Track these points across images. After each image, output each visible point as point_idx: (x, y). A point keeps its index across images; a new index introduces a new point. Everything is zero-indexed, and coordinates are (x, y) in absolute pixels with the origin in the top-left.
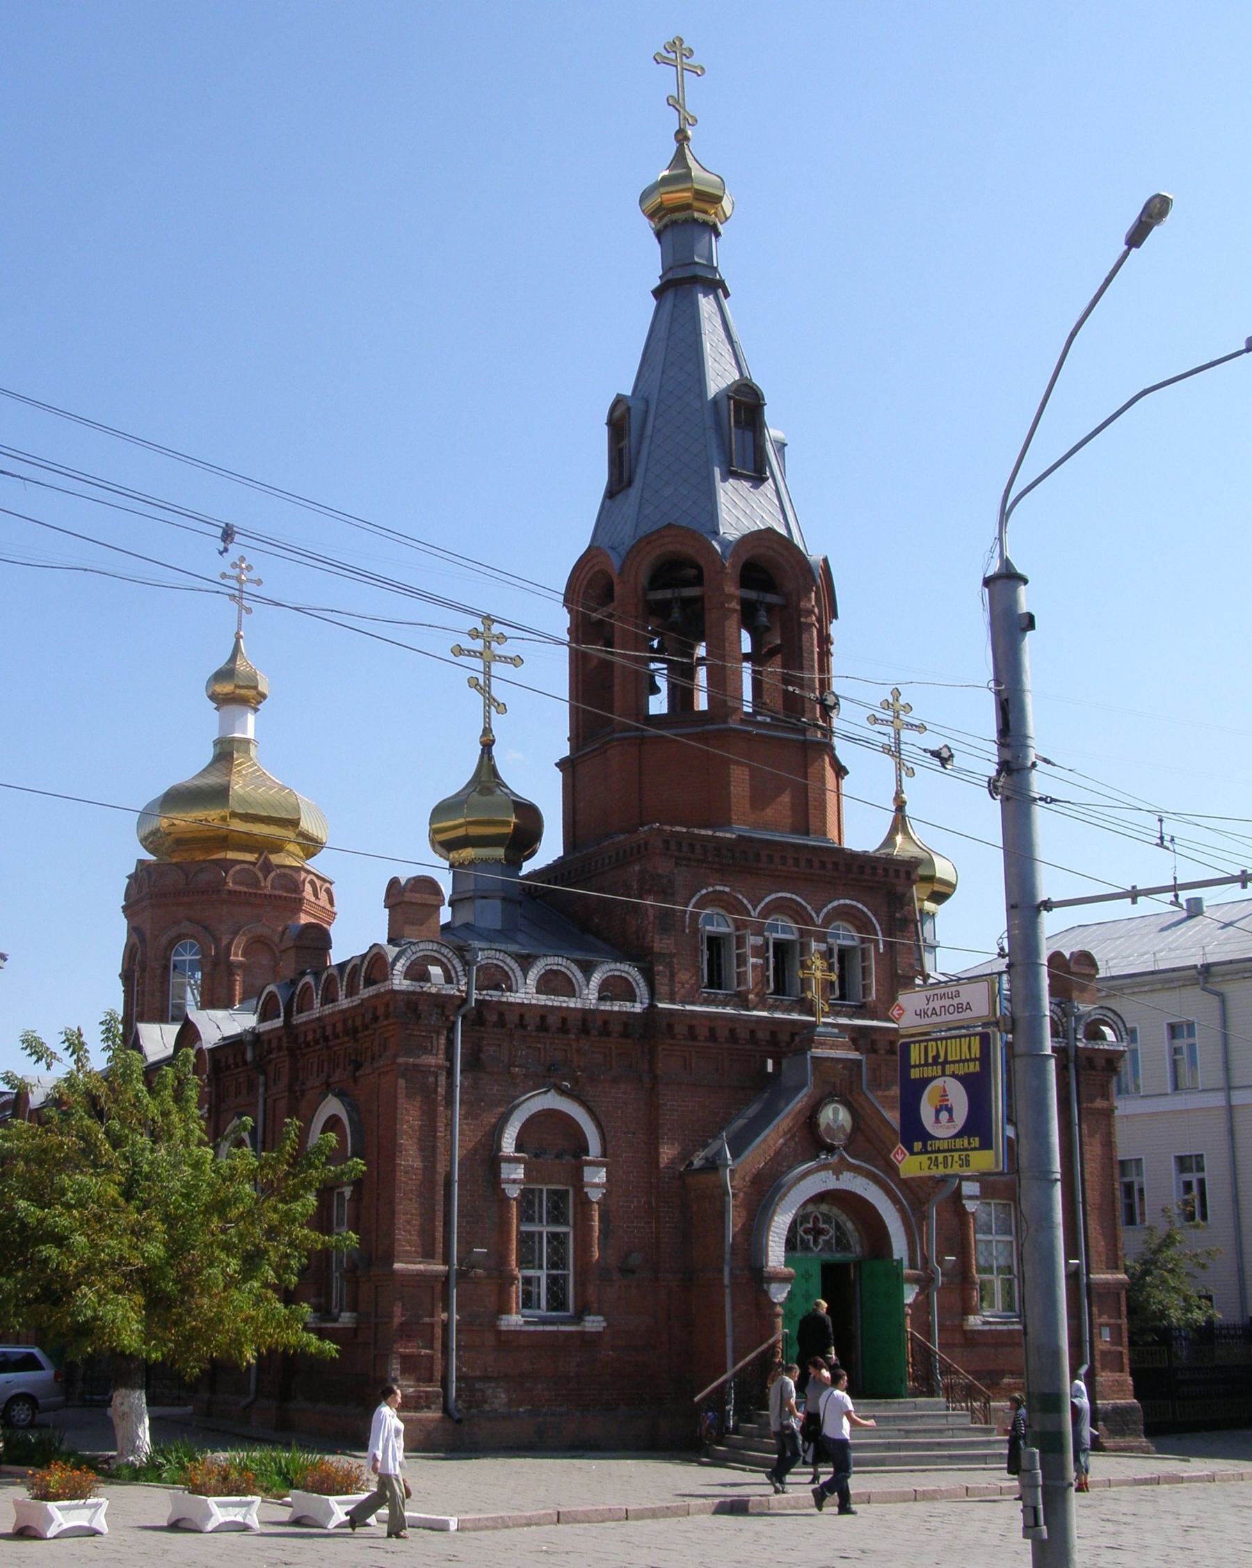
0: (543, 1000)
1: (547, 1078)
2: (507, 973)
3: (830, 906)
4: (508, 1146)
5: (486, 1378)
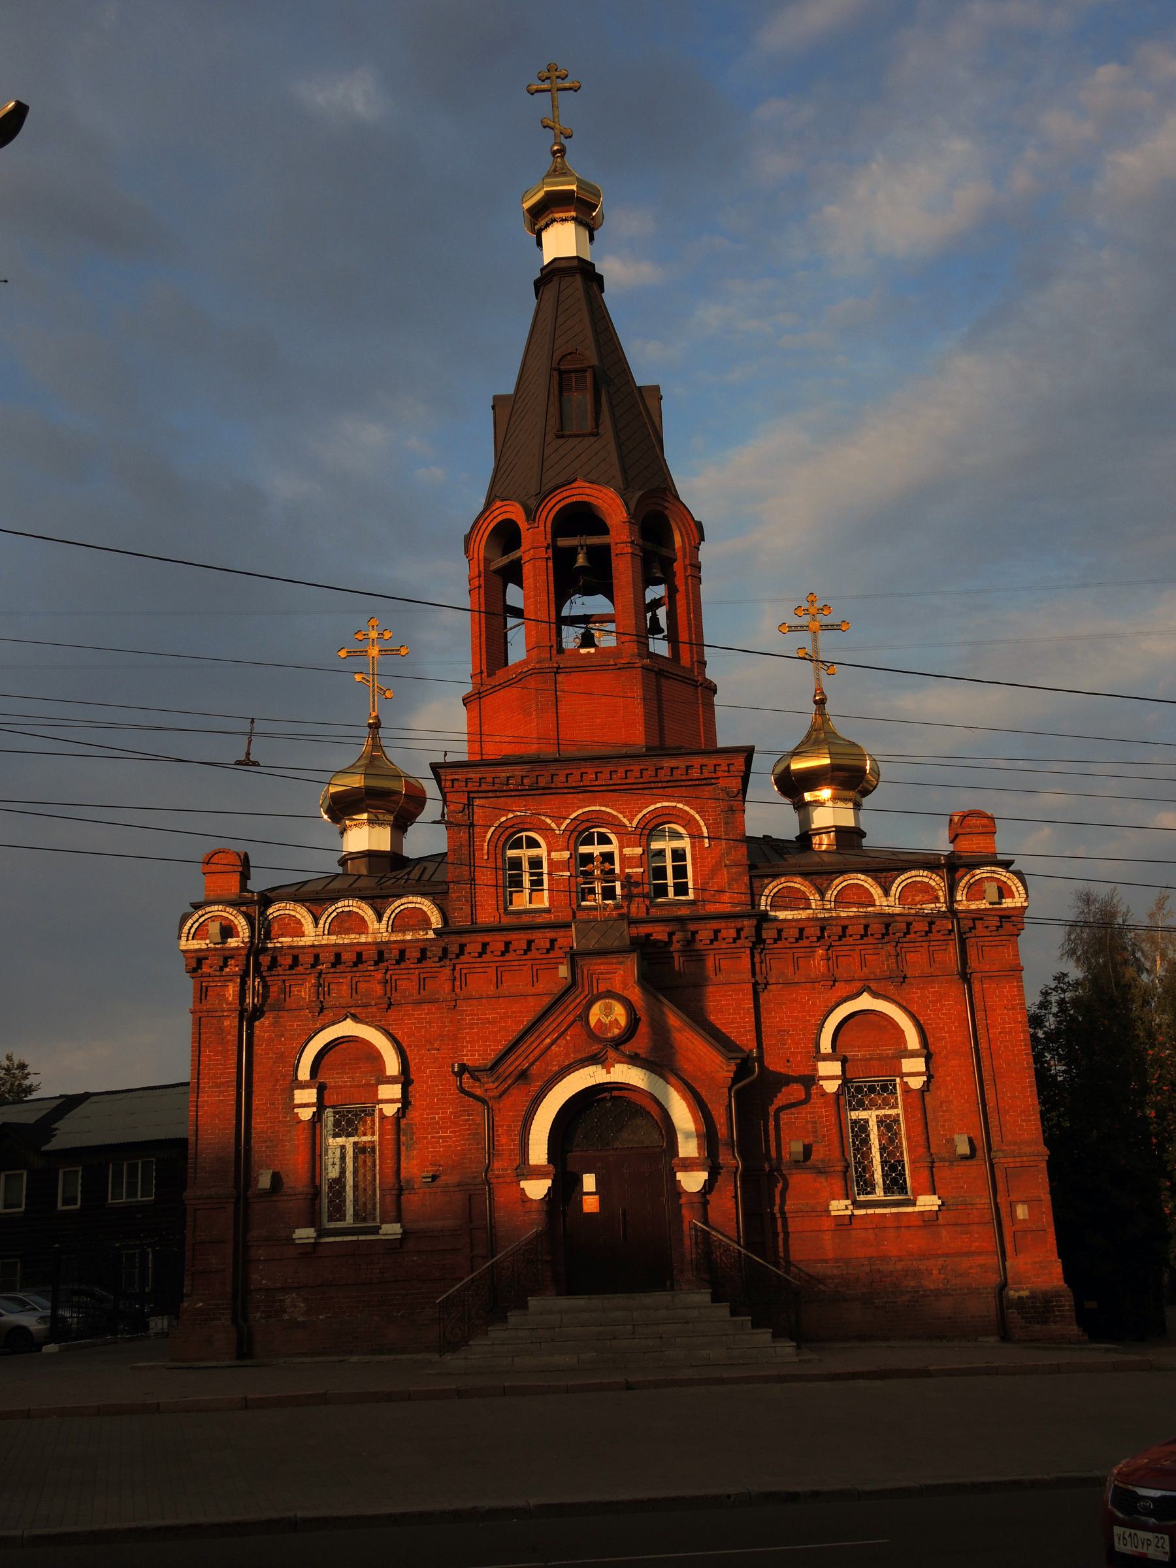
0: (333, 939)
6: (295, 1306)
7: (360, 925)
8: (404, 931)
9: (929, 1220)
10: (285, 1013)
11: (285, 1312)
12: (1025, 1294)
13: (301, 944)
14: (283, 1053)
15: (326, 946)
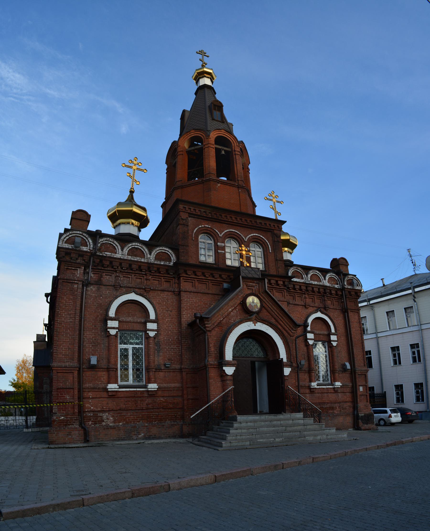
0: (130, 258)
1: (120, 289)
2: (115, 247)
3: (250, 236)
4: (112, 313)
5: (103, 411)
6: (108, 419)
7: (142, 255)
8: (161, 260)
9: (152, 394)
10: (103, 287)
11: (103, 421)
12: (363, 415)
13: (115, 256)
14: (101, 304)
15: (126, 260)
